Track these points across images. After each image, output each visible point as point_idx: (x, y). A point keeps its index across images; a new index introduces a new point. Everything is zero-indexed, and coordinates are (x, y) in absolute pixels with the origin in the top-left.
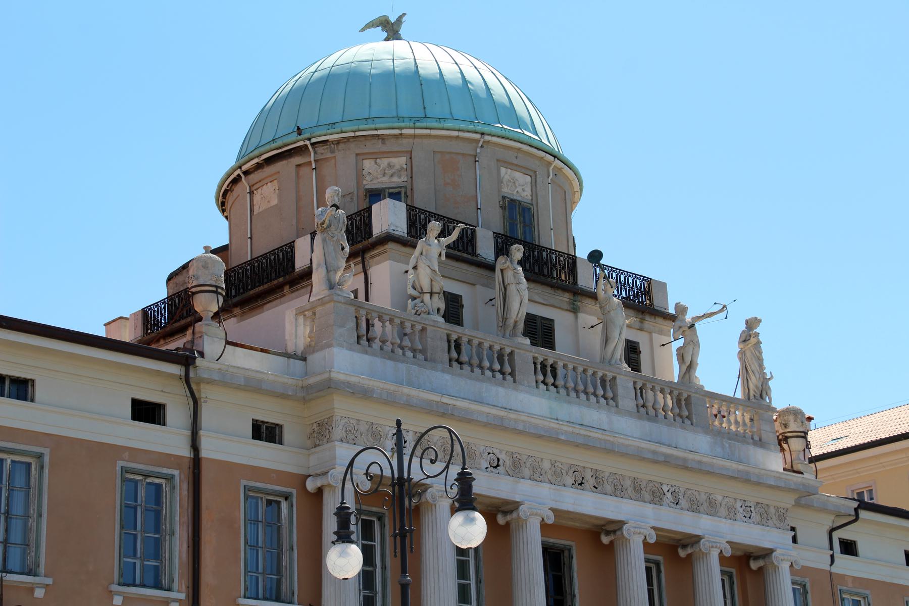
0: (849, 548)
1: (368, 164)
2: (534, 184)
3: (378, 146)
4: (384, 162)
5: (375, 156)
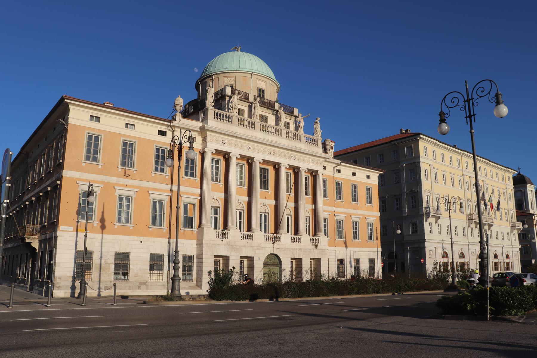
0: (339, 171)
1: (226, 79)
2: (266, 85)
3: (228, 74)
4: (229, 79)
5: (227, 77)
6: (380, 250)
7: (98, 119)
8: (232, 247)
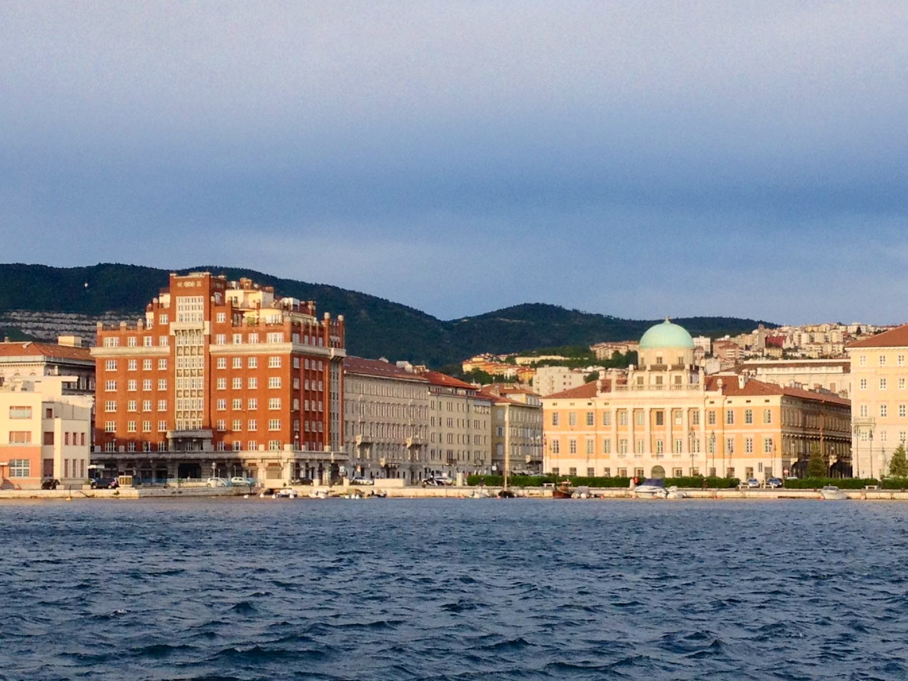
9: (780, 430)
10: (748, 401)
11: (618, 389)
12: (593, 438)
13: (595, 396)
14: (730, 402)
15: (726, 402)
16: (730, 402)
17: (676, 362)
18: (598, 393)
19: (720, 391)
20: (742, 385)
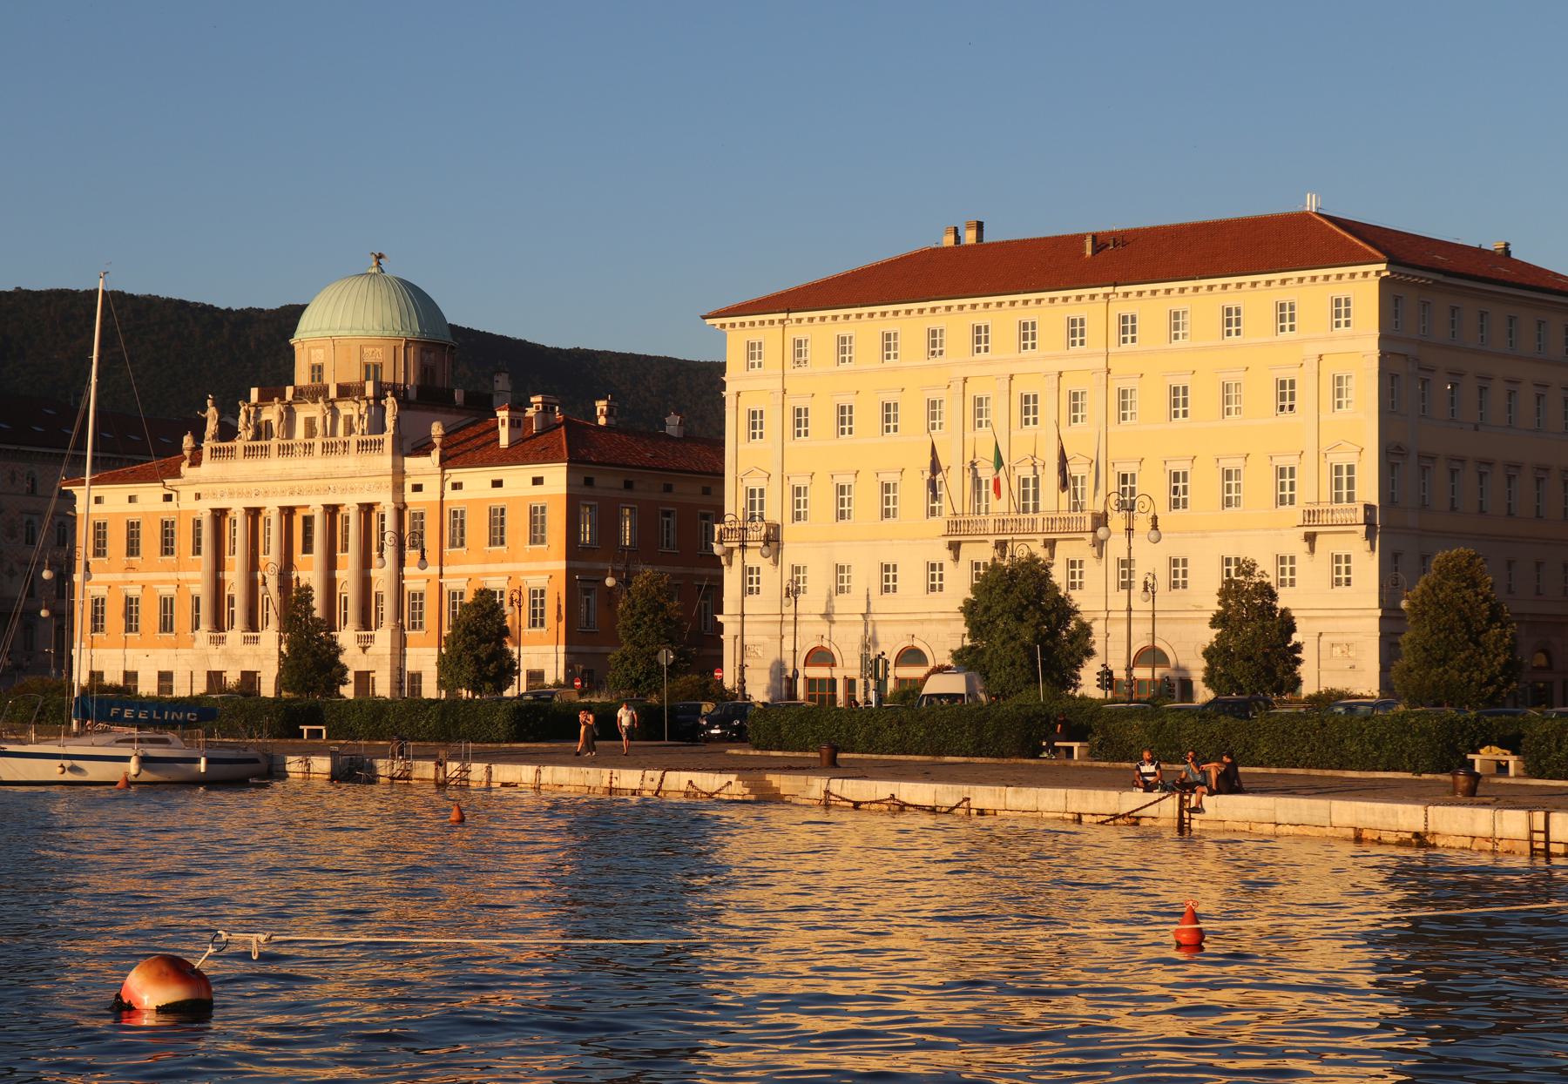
6: (562, 648)
7: (131, 499)
8: (228, 656)
9: (561, 565)
10: (497, 484)
11: (215, 452)
12: (168, 590)
13: (176, 474)
14: (457, 486)
15: (448, 485)
16: (457, 486)
17: (353, 376)
18: (184, 468)
19: (436, 455)
20: (504, 441)
